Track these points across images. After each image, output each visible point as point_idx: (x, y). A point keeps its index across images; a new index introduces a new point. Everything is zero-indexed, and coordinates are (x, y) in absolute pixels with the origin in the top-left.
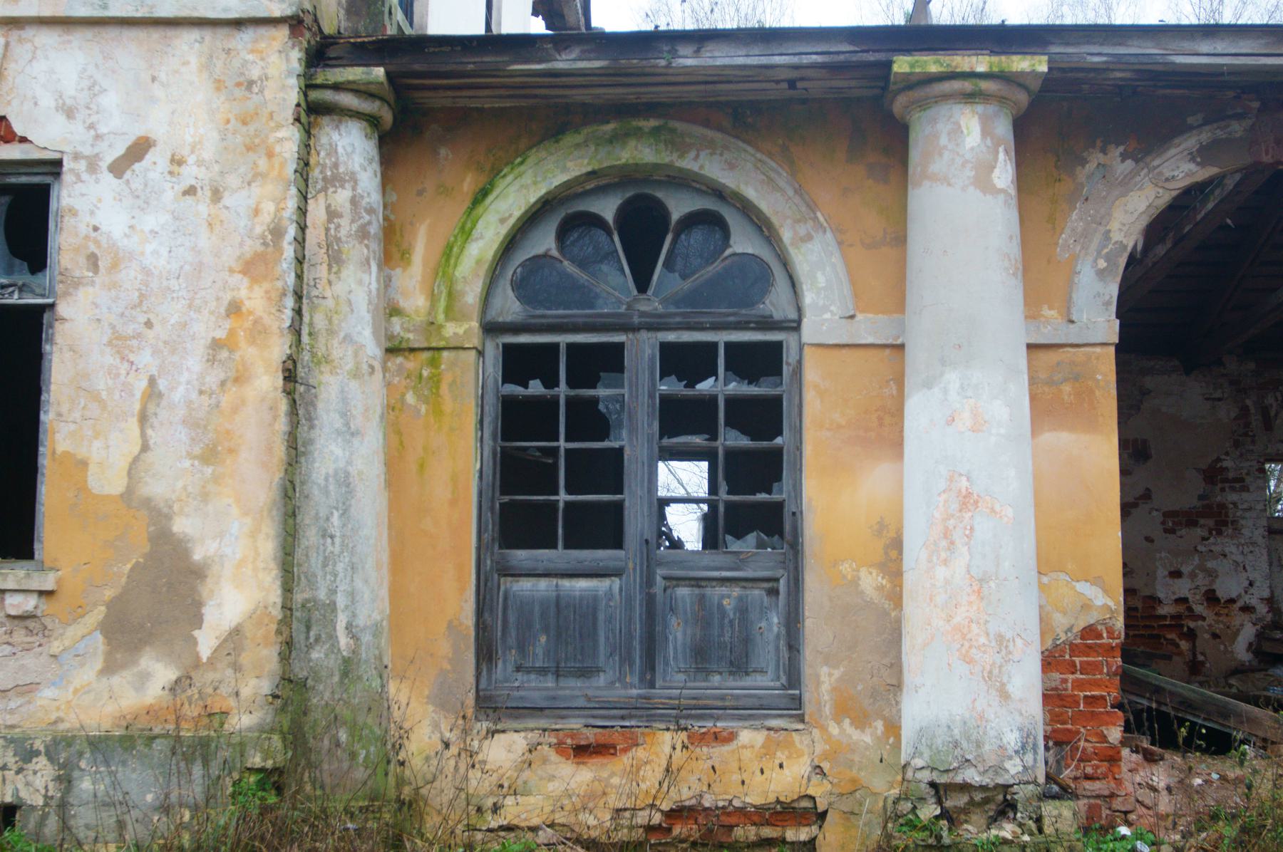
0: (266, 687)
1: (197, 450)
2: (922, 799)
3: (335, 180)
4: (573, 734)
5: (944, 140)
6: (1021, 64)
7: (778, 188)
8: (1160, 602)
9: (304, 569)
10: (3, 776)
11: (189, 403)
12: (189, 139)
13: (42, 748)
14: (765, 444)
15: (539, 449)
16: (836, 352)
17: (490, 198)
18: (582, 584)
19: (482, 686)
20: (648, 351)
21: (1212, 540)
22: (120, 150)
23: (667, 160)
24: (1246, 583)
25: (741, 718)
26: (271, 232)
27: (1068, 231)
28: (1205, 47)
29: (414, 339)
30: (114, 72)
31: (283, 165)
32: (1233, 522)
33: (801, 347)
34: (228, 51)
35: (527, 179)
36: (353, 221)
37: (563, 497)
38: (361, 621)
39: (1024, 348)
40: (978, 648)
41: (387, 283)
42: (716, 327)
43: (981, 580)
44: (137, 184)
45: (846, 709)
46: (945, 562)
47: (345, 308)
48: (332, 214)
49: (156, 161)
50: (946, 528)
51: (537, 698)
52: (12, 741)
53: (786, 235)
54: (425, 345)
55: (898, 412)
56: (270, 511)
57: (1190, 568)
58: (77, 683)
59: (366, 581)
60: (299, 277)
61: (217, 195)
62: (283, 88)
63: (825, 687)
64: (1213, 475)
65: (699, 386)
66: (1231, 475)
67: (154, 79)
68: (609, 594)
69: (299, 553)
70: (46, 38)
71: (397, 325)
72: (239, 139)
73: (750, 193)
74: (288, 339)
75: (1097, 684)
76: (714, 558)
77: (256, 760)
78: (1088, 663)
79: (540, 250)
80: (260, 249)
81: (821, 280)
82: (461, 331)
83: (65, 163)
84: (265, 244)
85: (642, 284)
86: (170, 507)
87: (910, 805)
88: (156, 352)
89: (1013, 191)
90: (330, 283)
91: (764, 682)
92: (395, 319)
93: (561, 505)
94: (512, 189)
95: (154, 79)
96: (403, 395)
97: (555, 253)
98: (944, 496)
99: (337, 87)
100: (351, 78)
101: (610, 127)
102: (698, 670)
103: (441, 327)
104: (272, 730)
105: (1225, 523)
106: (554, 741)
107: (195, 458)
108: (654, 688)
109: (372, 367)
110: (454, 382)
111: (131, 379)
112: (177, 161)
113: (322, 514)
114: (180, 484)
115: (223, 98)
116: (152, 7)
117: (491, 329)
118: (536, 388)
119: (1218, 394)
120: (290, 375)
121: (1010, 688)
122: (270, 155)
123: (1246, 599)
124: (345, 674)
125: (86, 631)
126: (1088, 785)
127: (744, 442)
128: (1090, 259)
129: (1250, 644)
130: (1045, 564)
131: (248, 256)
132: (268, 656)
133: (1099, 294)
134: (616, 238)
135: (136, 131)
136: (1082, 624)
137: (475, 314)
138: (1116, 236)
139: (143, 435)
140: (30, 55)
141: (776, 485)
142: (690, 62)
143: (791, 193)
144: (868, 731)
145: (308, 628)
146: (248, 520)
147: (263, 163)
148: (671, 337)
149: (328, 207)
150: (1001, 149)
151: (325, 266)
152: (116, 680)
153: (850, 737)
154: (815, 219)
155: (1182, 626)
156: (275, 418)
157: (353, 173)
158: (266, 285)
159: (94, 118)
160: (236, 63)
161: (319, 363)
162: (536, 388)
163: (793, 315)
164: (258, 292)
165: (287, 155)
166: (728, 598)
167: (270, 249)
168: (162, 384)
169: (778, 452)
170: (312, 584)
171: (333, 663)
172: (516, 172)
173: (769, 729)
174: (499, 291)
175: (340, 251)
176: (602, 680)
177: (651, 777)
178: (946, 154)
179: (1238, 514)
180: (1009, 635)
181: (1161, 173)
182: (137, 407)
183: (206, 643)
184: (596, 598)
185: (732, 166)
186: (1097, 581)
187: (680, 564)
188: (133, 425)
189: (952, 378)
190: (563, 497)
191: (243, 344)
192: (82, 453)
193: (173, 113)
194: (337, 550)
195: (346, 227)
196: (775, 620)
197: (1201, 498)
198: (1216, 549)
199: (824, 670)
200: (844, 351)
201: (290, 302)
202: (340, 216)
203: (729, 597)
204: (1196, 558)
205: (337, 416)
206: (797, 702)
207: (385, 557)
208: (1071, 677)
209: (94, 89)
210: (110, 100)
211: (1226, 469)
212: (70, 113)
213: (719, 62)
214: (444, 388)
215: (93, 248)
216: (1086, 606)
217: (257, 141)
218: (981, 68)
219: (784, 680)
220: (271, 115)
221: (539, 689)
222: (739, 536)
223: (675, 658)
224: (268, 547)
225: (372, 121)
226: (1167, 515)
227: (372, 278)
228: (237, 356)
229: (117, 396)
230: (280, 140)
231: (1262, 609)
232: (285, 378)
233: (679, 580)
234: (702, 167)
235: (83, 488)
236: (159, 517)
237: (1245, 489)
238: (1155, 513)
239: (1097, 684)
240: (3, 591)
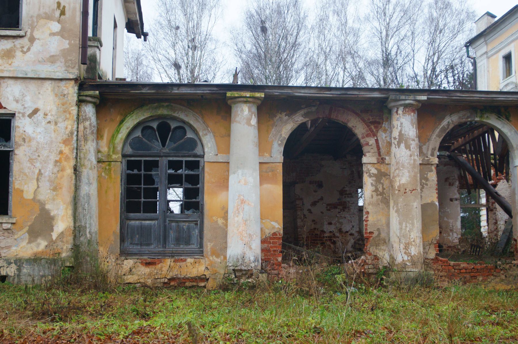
0: (70, 246)
1: (52, 188)
2: (231, 273)
3: (86, 119)
4: (145, 260)
5: (239, 113)
6: (258, 95)
7: (199, 122)
8: (325, 232)
9: (78, 218)
10: (508, 71)
11: (49, 176)
12: (49, 109)
13: (13, 262)
14: (195, 187)
15: (136, 187)
16: (213, 164)
17: (124, 122)
18: (148, 222)
19: (121, 248)
20: (165, 162)
21: (341, 213)
22: (30, 111)
23: (170, 113)
24: (351, 226)
25: (188, 256)
26: (70, 133)
27: (271, 134)
28: (303, 91)
29: (104, 159)
30: (29, 91)
31: (73, 116)
32: (348, 207)
33: (204, 162)
34: (58, 87)
35: (134, 117)
36: (90, 130)
37: (143, 200)
38: (93, 231)
39: (258, 164)
40: (245, 237)
41: (97, 143)
42: (182, 157)
43: (246, 221)
44: (35, 120)
45: (215, 253)
46: (237, 216)
47: (88, 152)
48: (85, 128)
49: (40, 114)
50: (238, 208)
51: (136, 251)
52: (5, 260)
53: (201, 134)
54: (107, 160)
55: (228, 180)
56: (70, 203)
57: (335, 222)
58: (21, 246)
59: (94, 221)
60: (77, 144)
61: (56, 123)
62: (73, 96)
63: (209, 248)
64: (342, 192)
65: (178, 172)
66: (348, 192)
67: (39, 93)
68: (154, 225)
69: (77, 214)
70: (11, 82)
71: (100, 155)
72: (62, 109)
73: (192, 122)
74: (75, 160)
75: (276, 247)
76: (183, 216)
77: (68, 264)
78: (274, 242)
79: (137, 135)
80: (67, 137)
81: (209, 145)
82: (117, 157)
83: (16, 114)
84: (69, 136)
85: (164, 145)
86: (45, 202)
87: (228, 275)
88: (41, 163)
89: (256, 125)
90: (84, 146)
91: (194, 247)
92: (99, 154)
93: (142, 202)
94: (130, 120)
95: (39, 93)
96: (101, 173)
97: (141, 136)
98: (237, 200)
99: (86, 96)
100: (90, 94)
101: (156, 105)
102: (177, 244)
103: (111, 156)
104: (72, 257)
105: (346, 208)
106: (140, 261)
107: (51, 190)
108: (166, 248)
109: (94, 167)
110: (115, 170)
111: (34, 170)
112: (46, 115)
113: (83, 204)
114: (47, 196)
115: (57, 99)
116: (39, 75)
117: (124, 156)
118: (136, 172)
119: (344, 167)
120: (75, 169)
121: (252, 247)
122: (70, 113)
123: (352, 232)
124: (89, 244)
125: (23, 233)
126: (273, 271)
127: (190, 186)
128: (276, 141)
129: (352, 245)
130: (263, 217)
131: (64, 139)
132: (70, 239)
133: (278, 150)
134: (157, 133)
135: (35, 107)
136: (272, 232)
137: (120, 153)
138: (283, 135)
139: (38, 184)
140: (6, 86)
141: (197, 197)
142: (176, 91)
143: (202, 123)
144: (219, 258)
145: (80, 232)
146: (65, 205)
147: (68, 116)
148: (171, 159)
149: (84, 126)
150: (253, 115)
151: (83, 141)
152: (32, 245)
153: (215, 260)
154: (208, 130)
155: (332, 240)
156: (72, 180)
157: (90, 117)
158: (69, 147)
159: (24, 103)
160: (61, 90)
161: (82, 166)
162: (136, 172)
163: (202, 154)
164: (67, 148)
165: (74, 114)
166: (185, 226)
167: (70, 138)
168: (42, 171)
169: (198, 189)
170: (80, 221)
171: (85, 241)
172: (131, 116)
173: (195, 258)
174: (126, 146)
175: (87, 138)
176: (152, 246)
177: (165, 269)
178: (240, 116)
179: (350, 204)
180: (252, 234)
181: (294, 120)
182: (36, 177)
183: (54, 236)
184: (151, 226)
185: (187, 116)
186: (276, 221)
187: (173, 217)
188: (35, 182)
189: (240, 172)
190: (143, 200)
191: (63, 161)
192: (22, 188)
193: (44, 102)
194: (87, 213)
195: (88, 131)
196: (197, 231)
197: (338, 200)
198: (343, 216)
199: (209, 243)
200: (215, 163)
201: (75, 151)
202: (87, 128)
203: (185, 225)
204: (337, 219)
205: (86, 179)
206: (202, 252)
207: (97, 215)
208: (270, 245)
209: (23, 95)
210: (28, 98)
211: (346, 191)
212: (17, 101)
213: (184, 92)
214: (112, 172)
215: (24, 136)
216: (274, 228)
217: (66, 110)
218: (248, 96)
219: (199, 246)
220: (70, 104)
221: (137, 249)
222: (188, 210)
223: (171, 241)
224: (70, 212)
225: (94, 103)
226: (328, 205)
227: (94, 144)
228: (62, 164)
229: (31, 174)
230: (72, 110)
231: (356, 235)
232: (74, 170)
233: (172, 221)
234: (179, 116)
235: (22, 197)
236: (42, 205)
237: (352, 197)
238: (324, 204)
239: (276, 247)
240: (2, 223)
